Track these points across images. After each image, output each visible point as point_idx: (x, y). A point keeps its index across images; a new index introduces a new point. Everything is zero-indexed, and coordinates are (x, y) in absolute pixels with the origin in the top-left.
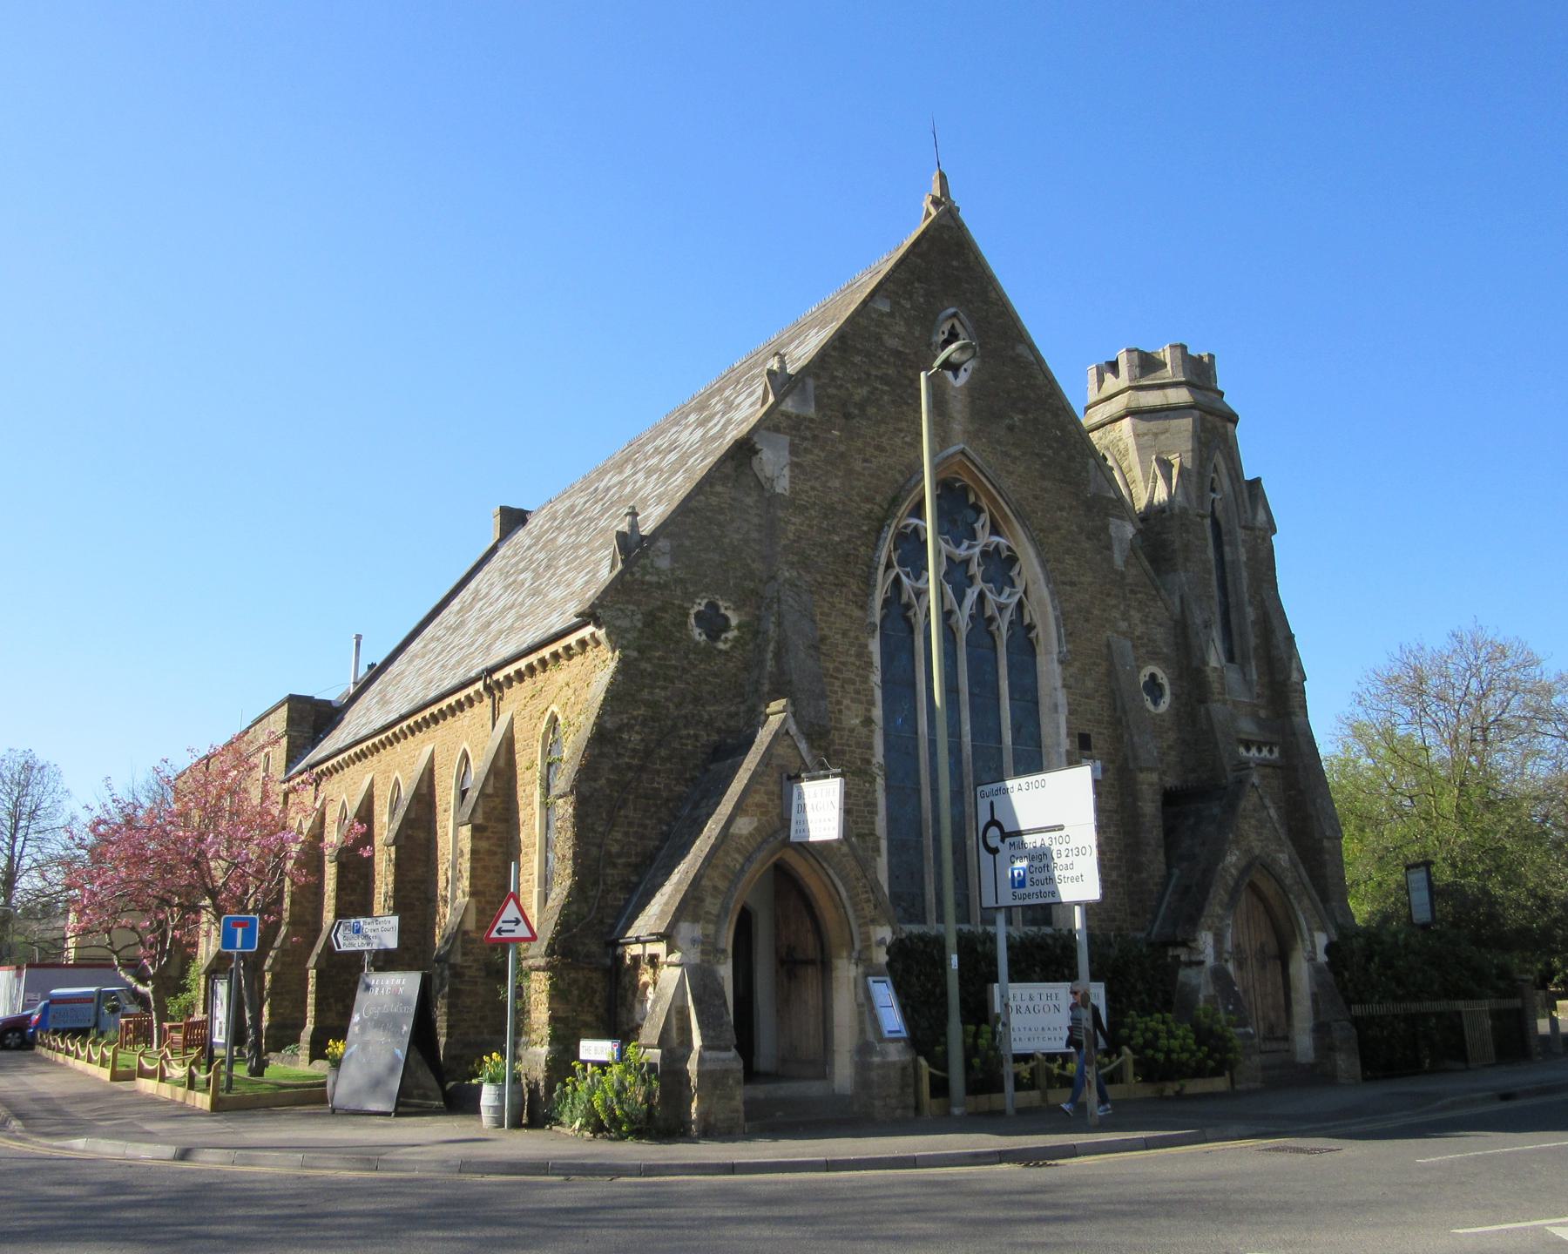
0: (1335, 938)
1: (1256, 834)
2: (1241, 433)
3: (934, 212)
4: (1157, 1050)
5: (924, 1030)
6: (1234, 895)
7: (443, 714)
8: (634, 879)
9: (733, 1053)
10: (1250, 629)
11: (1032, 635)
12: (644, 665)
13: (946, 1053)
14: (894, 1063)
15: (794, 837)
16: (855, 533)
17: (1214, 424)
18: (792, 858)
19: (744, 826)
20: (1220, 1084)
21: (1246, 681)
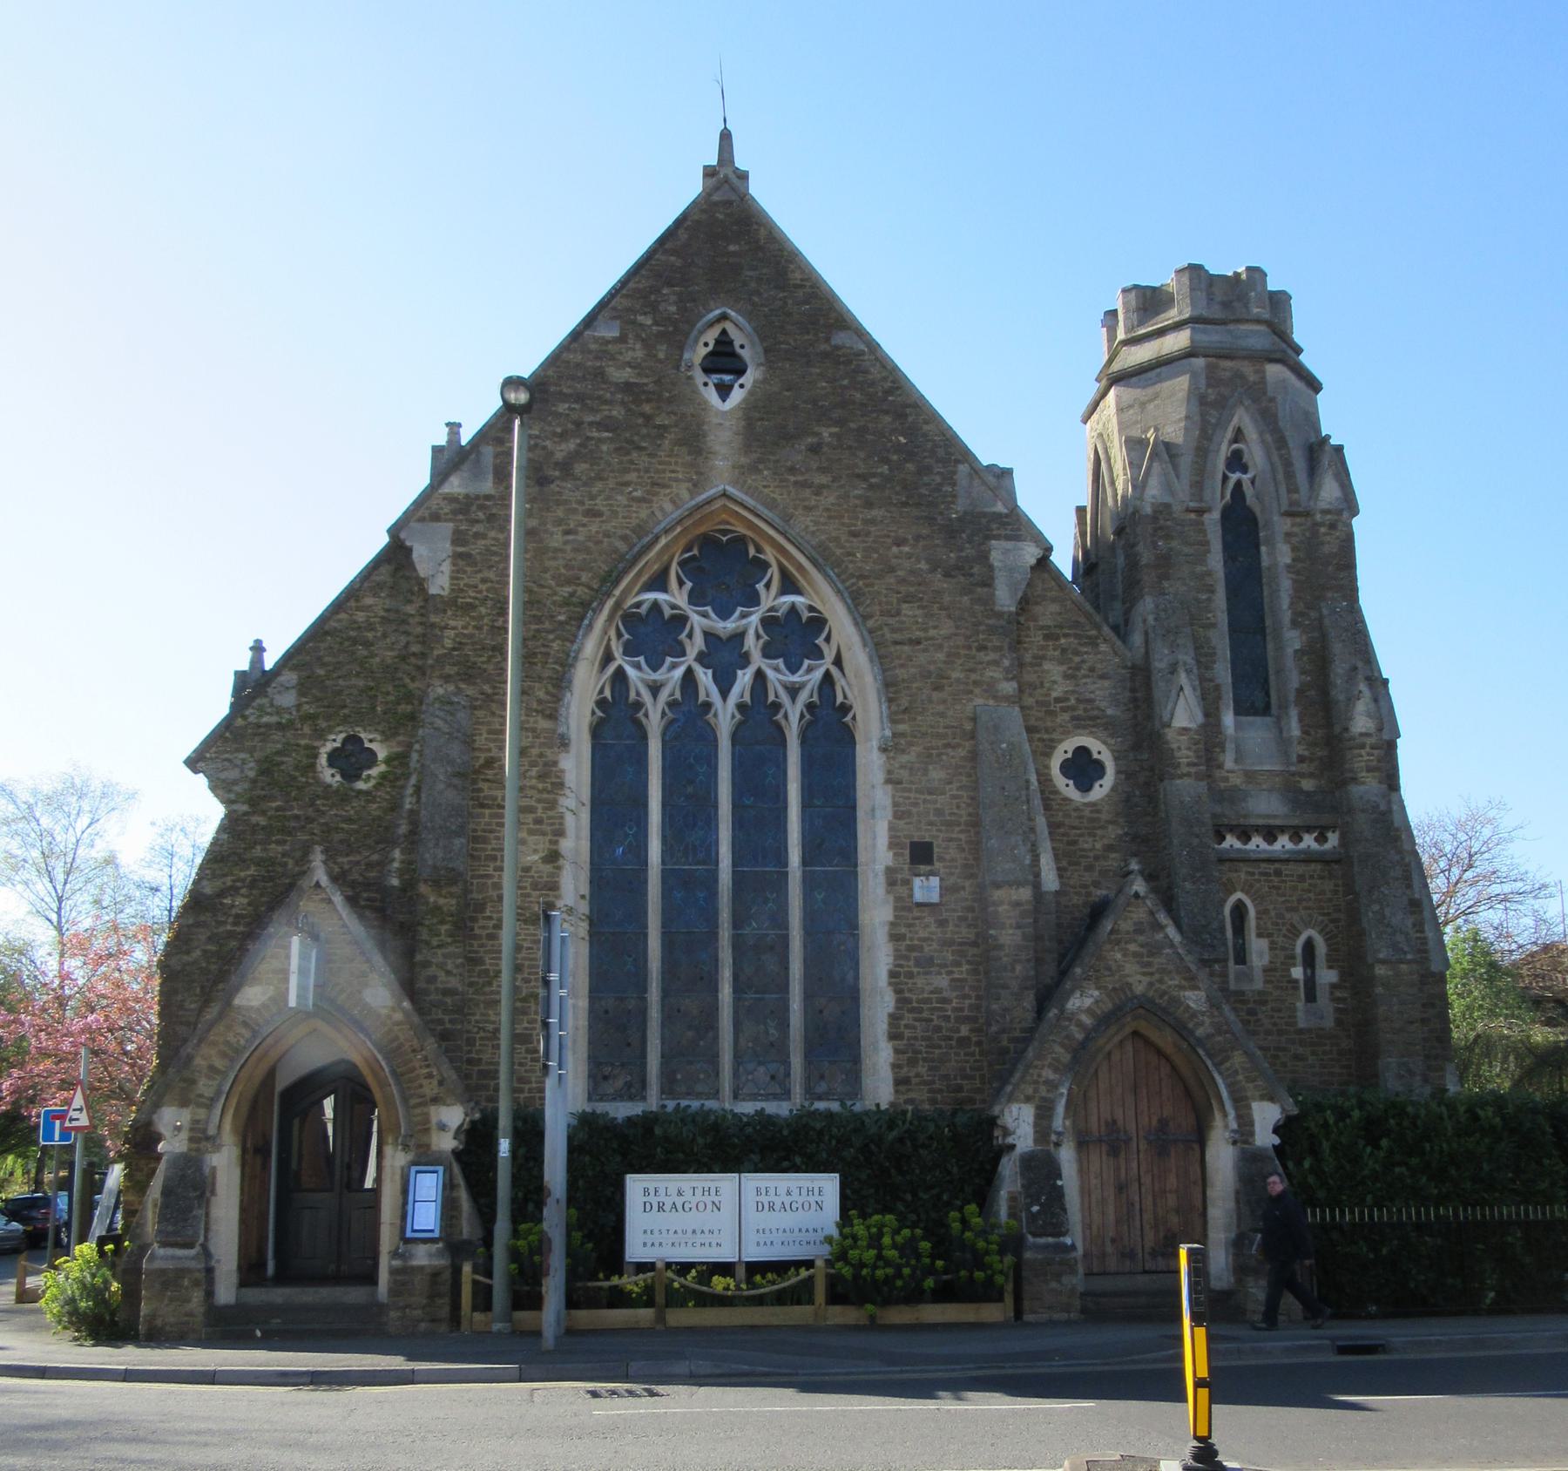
10: (1290, 662)
14: (422, 1268)
16: (547, 625)
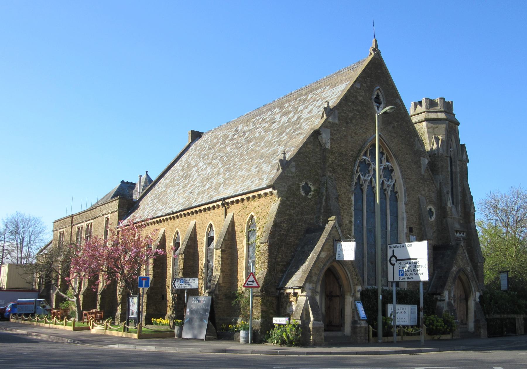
0: (482, 294)
1: (461, 261)
2: (460, 127)
3: (373, 54)
4: (433, 326)
5: (371, 319)
6: (454, 279)
7: (201, 211)
8: (284, 269)
9: (321, 322)
11: (397, 195)
12: (287, 202)
13: (377, 325)
15: (337, 258)
16: (348, 161)
17: (452, 125)
18: (335, 264)
19: (323, 255)
20: (449, 337)
21: (457, 211)
